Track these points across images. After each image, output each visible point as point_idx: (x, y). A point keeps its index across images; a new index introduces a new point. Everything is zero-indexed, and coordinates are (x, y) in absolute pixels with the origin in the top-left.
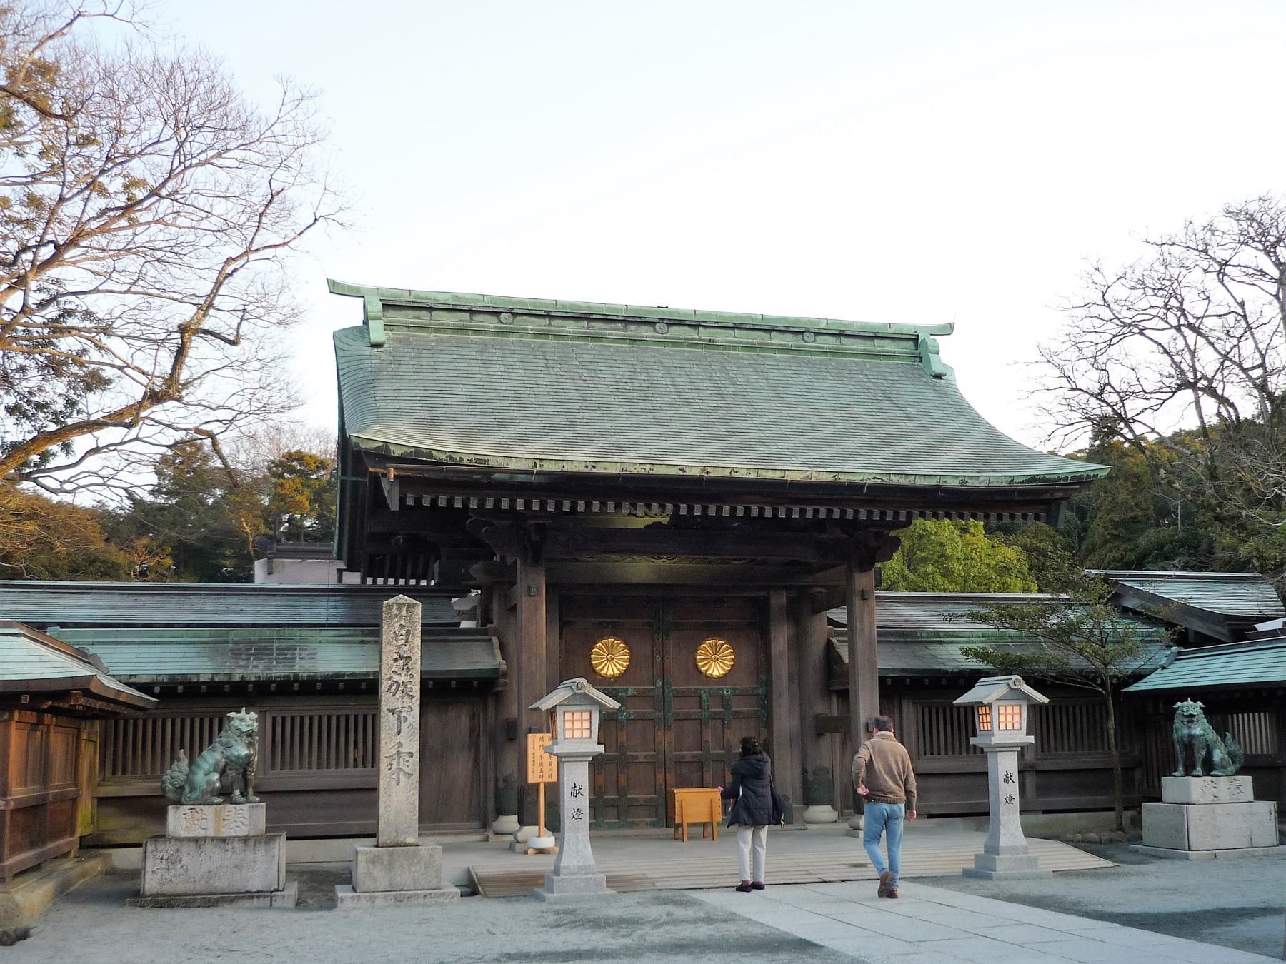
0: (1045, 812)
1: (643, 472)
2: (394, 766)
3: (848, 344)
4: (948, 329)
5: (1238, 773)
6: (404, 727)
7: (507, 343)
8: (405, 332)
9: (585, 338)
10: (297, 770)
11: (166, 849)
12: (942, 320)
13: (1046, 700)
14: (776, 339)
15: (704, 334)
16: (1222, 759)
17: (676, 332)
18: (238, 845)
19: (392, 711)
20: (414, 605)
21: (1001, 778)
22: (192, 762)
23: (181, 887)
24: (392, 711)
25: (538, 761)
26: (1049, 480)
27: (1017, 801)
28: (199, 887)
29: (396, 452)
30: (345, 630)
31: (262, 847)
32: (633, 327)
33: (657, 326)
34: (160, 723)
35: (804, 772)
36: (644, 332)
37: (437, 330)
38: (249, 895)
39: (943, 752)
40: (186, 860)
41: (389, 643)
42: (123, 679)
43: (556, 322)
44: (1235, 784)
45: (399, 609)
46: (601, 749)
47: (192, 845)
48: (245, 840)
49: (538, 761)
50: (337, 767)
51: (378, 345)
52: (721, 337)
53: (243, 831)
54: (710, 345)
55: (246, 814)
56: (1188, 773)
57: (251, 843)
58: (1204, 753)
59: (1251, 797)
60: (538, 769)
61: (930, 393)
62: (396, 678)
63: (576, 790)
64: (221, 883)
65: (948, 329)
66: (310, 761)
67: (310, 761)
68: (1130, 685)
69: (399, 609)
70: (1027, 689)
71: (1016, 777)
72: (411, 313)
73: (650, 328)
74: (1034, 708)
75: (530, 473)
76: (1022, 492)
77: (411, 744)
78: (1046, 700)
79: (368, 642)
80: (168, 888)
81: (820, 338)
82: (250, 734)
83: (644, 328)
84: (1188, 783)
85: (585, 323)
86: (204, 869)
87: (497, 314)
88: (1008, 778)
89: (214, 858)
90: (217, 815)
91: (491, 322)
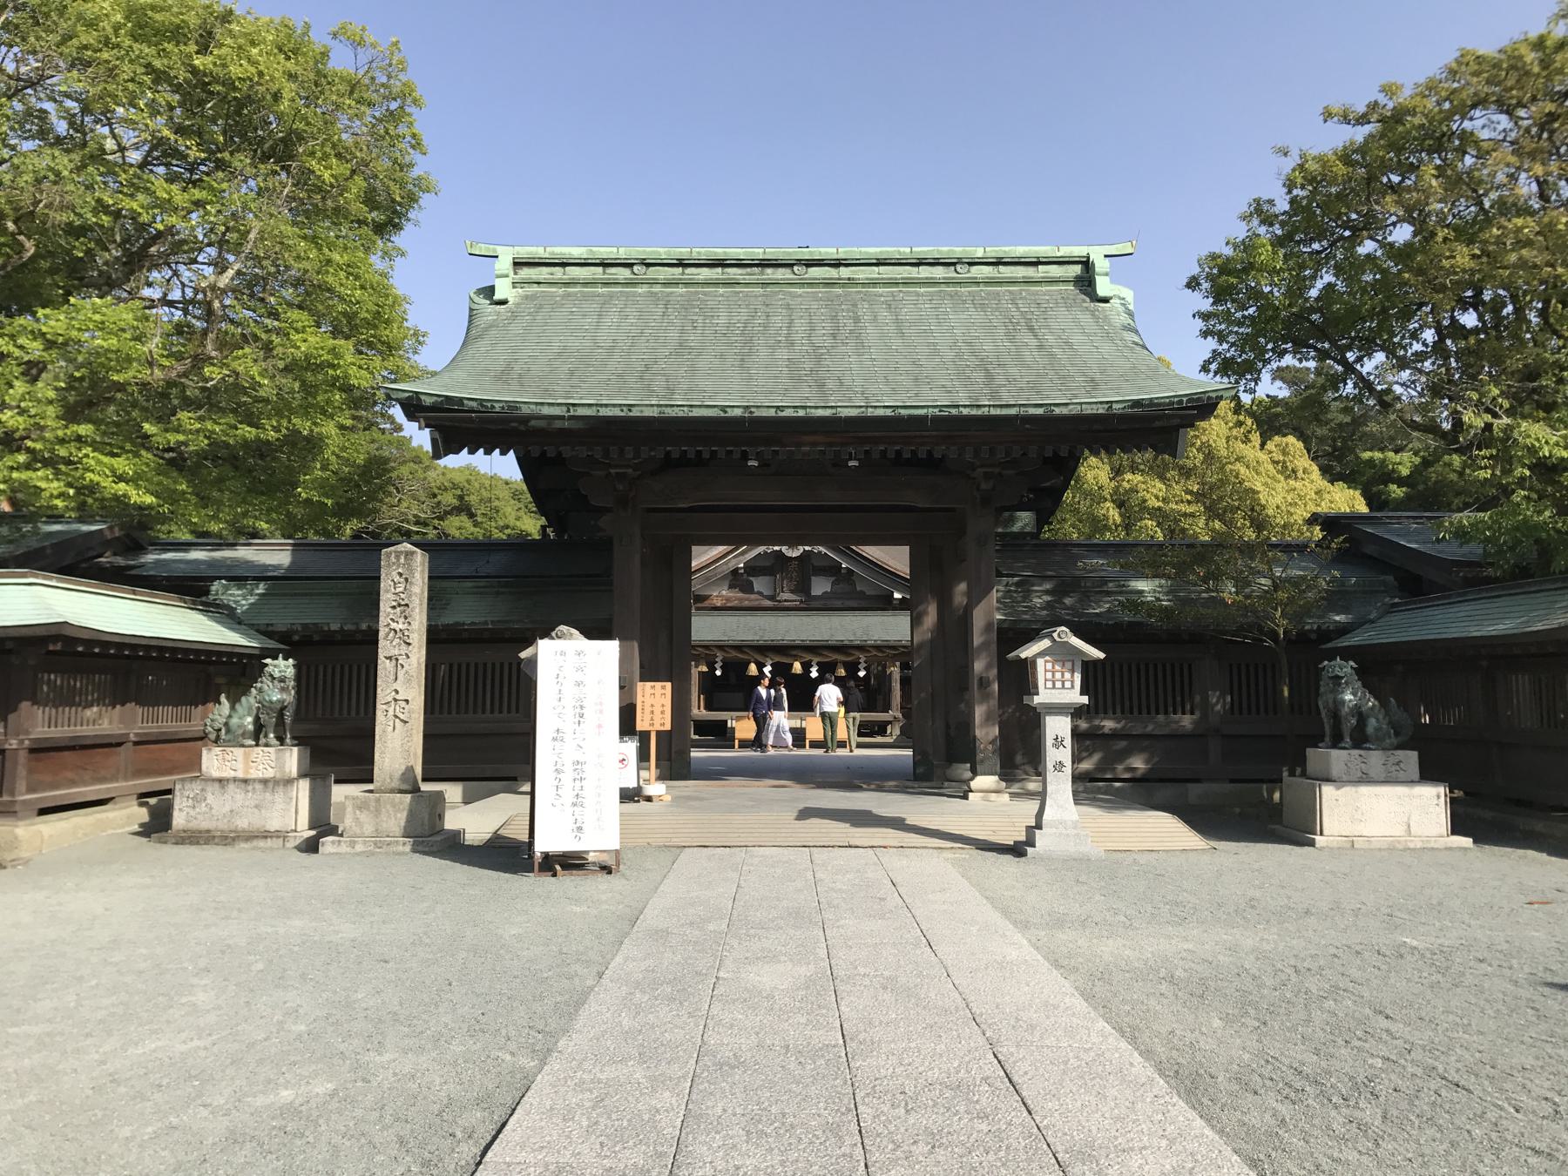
0: (1232, 781)
1: (681, 414)
2: (391, 713)
3: (1007, 271)
5: (1401, 747)
6: (401, 673)
7: (635, 294)
8: (535, 288)
9: (716, 284)
10: (496, 714)
11: (195, 788)
13: (1102, 655)
14: (925, 272)
15: (845, 272)
16: (1377, 730)
17: (815, 272)
18: (258, 786)
19: (390, 658)
20: (413, 553)
21: (1049, 742)
22: (233, 708)
23: (205, 825)
24: (390, 658)
25: (648, 709)
26: (1159, 405)
27: (1068, 770)
28: (223, 825)
29: (428, 401)
30: (483, 582)
31: (280, 789)
32: (769, 271)
34: (355, 668)
35: (948, 726)
36: (781, 274)
37: (567, 284)
38: (266, 835)
39: (1136, 710)
40: (210, 798)
41: (387, 591)
42: (262, 628)
43: (689, 270)
44: (1392, 759)
45: (398, 557)
46: (1085, 700)
47: (217, 785)
48: (265, 782)
49: (648, 709)
50: (475, 712)
51: (503, 302)
52: (862, 273)
53: (270, 773)
54: (851, 282)
55: (273, 757)
56: (1334, 746)
57: (271, 785)
58: (1354, 721)
59: (1417, 776)
60: (647, 716)
61: (1085, 318)
62: (394, 625)
63: (1058, 742)
64: (242, 823)
66: (441, 707)
67: (441, 707)
68: (1330, 640)
69: (398, 557)
70: (1076, 642)
71: (1068, 742)
72: (545, 270)
73: (788, 270)
74: (1089, 667)
75: (561, 418)
76: (1122, 417)
77: (415, 694)
78: (1102, 655)
80: (194, 825)
81: (974, 269)
82: (282, 680)
83: (781, 270)
84: (1328, 755)
85: (719, 270)
86: (227, 808)
87: (630, 265)
88: (1058, 742)
89: (236, 798)
90: (246, 756)
91: (624, 273)
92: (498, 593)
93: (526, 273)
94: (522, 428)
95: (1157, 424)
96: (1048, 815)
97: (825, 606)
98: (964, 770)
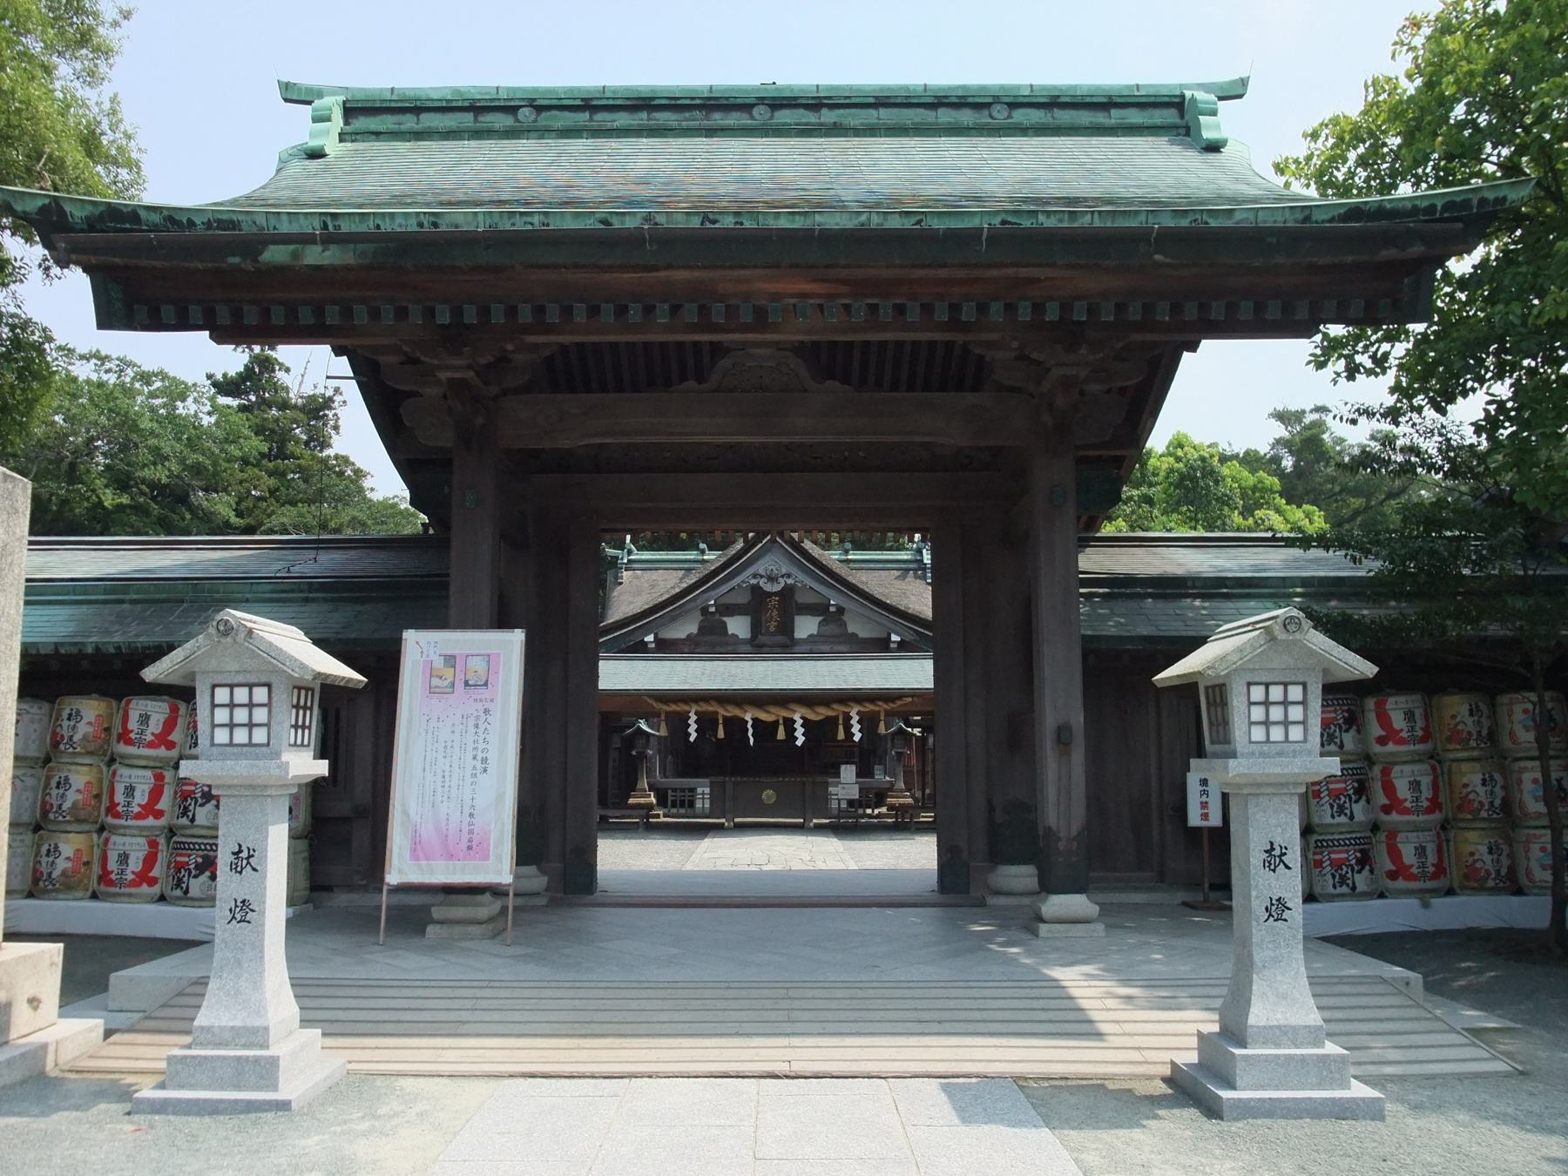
4: (1234, 92)
12: (1225, 75)
33: (755, 112)
65: (1234, 92)
73: (745, 115)
79: (314, 600)
85: (644, 115)
92: (306, 600)
93: (361, 123)
94: (248, 265)
95: (1387, 254)
96: (1259, 1014)
97: (814, 649)
98: (1020, 876)
